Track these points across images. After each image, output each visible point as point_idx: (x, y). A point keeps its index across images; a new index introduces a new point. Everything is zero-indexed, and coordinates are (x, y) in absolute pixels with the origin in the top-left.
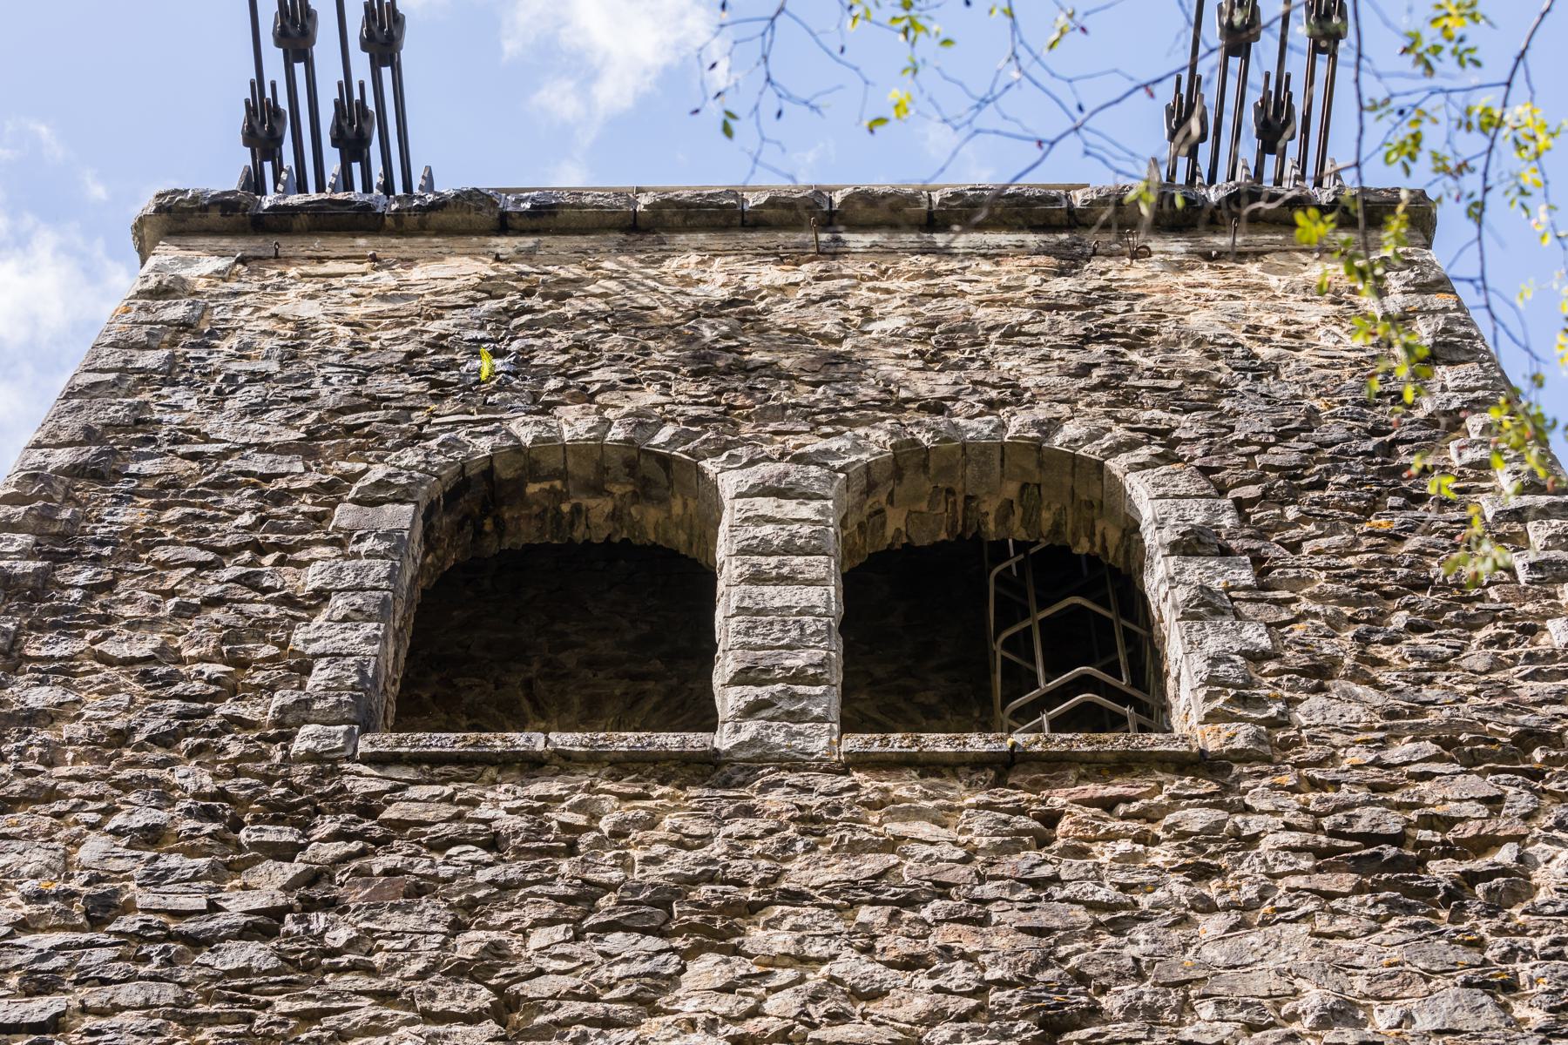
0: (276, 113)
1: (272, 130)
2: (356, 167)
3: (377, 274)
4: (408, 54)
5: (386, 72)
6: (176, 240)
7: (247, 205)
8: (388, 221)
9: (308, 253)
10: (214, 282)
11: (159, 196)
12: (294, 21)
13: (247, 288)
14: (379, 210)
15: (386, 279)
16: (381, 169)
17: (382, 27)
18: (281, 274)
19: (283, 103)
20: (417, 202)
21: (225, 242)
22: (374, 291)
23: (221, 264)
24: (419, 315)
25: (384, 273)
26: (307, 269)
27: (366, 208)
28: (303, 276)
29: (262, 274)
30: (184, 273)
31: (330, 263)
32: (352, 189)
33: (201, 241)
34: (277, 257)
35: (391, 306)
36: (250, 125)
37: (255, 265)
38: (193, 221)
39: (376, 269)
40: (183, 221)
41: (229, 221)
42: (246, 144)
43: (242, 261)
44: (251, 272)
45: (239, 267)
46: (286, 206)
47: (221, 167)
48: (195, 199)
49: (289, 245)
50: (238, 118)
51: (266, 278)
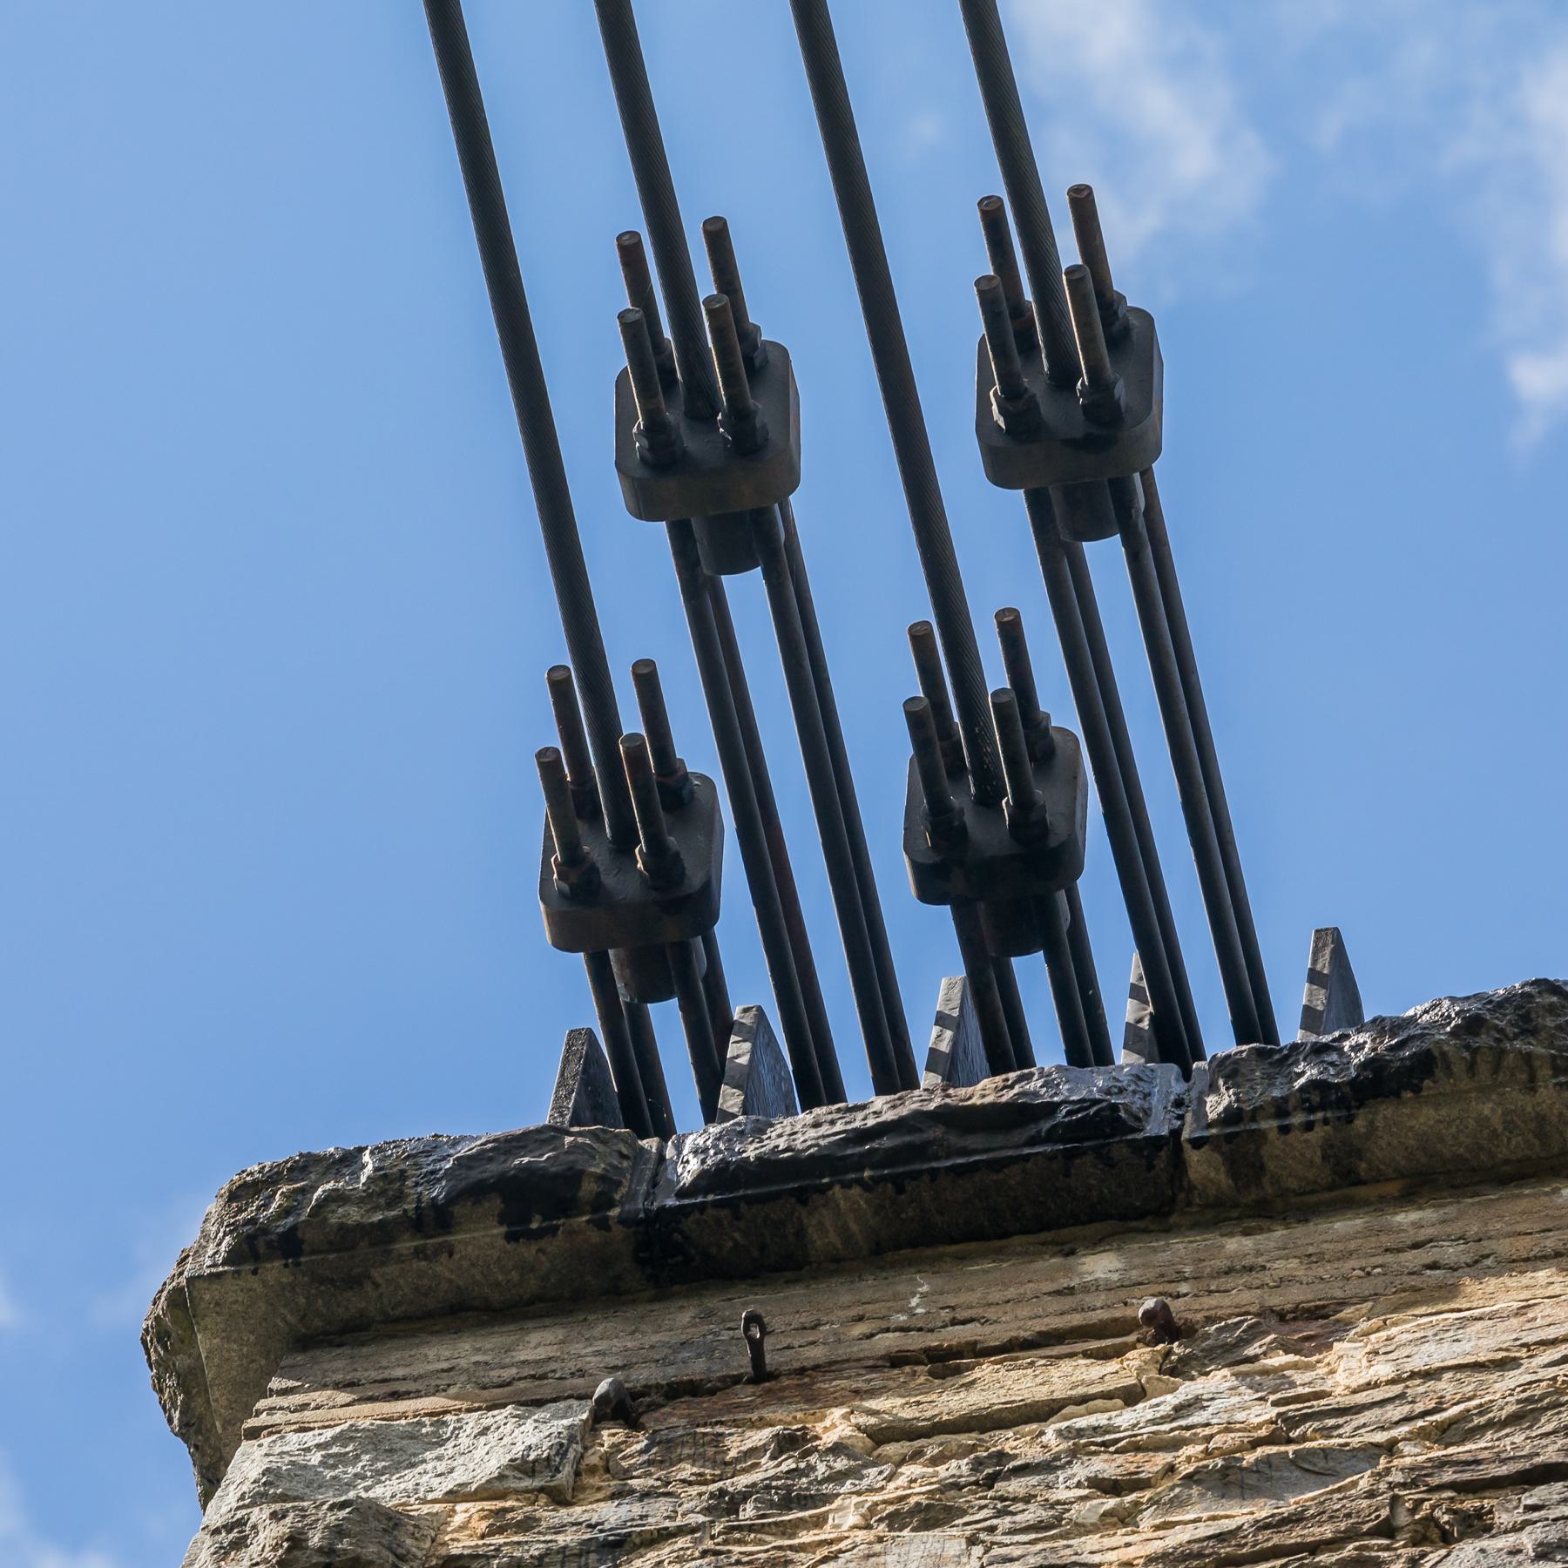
0: (674, 794)
1: (665, 866)
2: (1031, 976)
3: (1187, 1390)
4: (1186, 475)
5: (1106, 560)
6: (337, 1363)
7: (609, 1182)
8: (1202, 1167)
9: (888, 1342)
10: (518, 1508)
11: (240, 1193)
12: (701, 408)
13: (657, 1514)
14: (1158, 1126)
15: (1227, 1402)
16: (1134, 969)
17: (1063, 376)
18: (789, 1443)
19: (697, 749)
20: (1308, 1072)
21: (537, 1345)
22: (1188, 1457)
23: (530, 1434)
24: (1387, 1529)
25: (1218, 1380)
26: (892, 1406)
27: (1102, 1125)
28: (880, 1435)
29: (711, 1454)
30: (387, 1492)
31: (985, 1371)
32: (1024, 1059)
33: (437, 1354)
34: (761, 1374)
35: (1263, 1509)
36: (573, 859)
37: (674, 1419)
38: (400, 1275)
39: (1179, 1370)
40: (354, 1282)
41: (543, 1256)
42: (566, 940)
43: (621, 1409)
44: (666, 1451)
45: (609, 1436)
46: (769, 1166)
47: (475, 1040)
48: (389, 1183)
49: (804, 1321)
50: (518, 829)
51: (730, 1468)
